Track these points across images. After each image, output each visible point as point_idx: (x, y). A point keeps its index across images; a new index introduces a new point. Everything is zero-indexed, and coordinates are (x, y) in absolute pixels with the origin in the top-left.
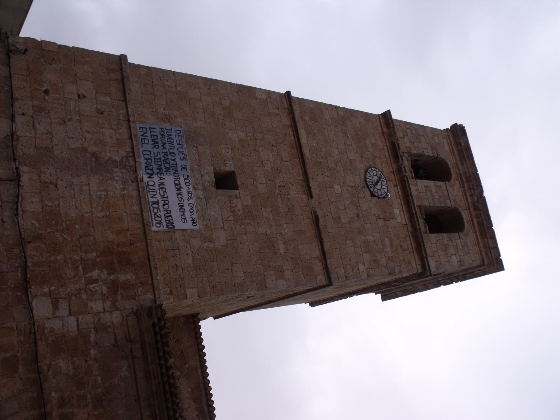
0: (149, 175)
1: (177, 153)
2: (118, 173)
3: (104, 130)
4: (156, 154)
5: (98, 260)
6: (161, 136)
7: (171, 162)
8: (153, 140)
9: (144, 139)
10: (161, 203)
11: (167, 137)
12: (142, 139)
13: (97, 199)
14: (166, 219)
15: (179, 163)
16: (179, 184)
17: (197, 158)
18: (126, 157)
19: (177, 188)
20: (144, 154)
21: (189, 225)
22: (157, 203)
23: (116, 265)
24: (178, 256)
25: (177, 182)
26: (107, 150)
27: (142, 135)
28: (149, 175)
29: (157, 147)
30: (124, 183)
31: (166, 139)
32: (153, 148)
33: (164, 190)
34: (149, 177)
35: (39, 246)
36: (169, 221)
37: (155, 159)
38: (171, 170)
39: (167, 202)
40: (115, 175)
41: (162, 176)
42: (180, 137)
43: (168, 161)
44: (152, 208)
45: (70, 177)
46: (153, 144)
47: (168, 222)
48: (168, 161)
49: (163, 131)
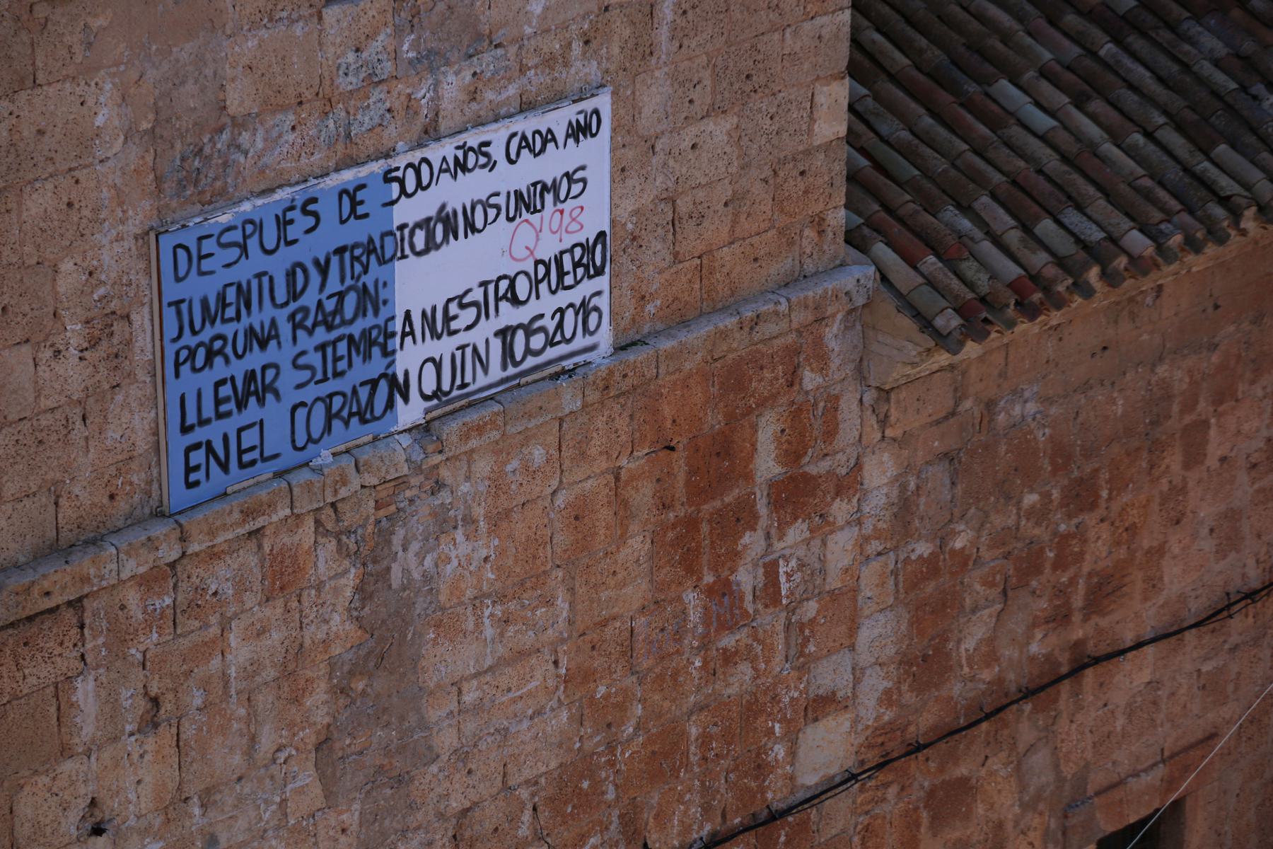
0: (399, 400)
1: (287, 256)
2: (407, 563)
3: (233, 671)
4: (306, 375)
5: (709, 578)
6: (218, 360)
7: (334, 285)
8: (241, 405)
9: (241, 452)
10: (509, 315)
11: (219, 328)
12: (242, 465)
13: (511, 630)
14: (569, 280)
15: (332, 235)
16: (425, 224)
17: (291, 118)
18: (337, 536)
19: (446, 239)
20: (310, 439)
21: (595, 155)
22: (505, 334)
23: (727, 500)
24: (701, 195)
25: (420, 239)
26: (321, 635)
27: (225, 467)
28: (399, 400)
29: (270, 374)
30: (443, 523)
31: (228, 330)
32: (277, 395)
33: (453, 309)
34: (406, 399)
35: (657, 817)
36: (576, 265)
37: (325, 379)
38: (368, 280)
39: (504, 285)
40: (416, 575)
41: (398, 326)
42: (208, 246)
43: (330, 305)
44: (531, 362)
45: (434, 768)
46: (261, 401)
47: (580, 271)
48: (330, 305)
49: (192, 354)
